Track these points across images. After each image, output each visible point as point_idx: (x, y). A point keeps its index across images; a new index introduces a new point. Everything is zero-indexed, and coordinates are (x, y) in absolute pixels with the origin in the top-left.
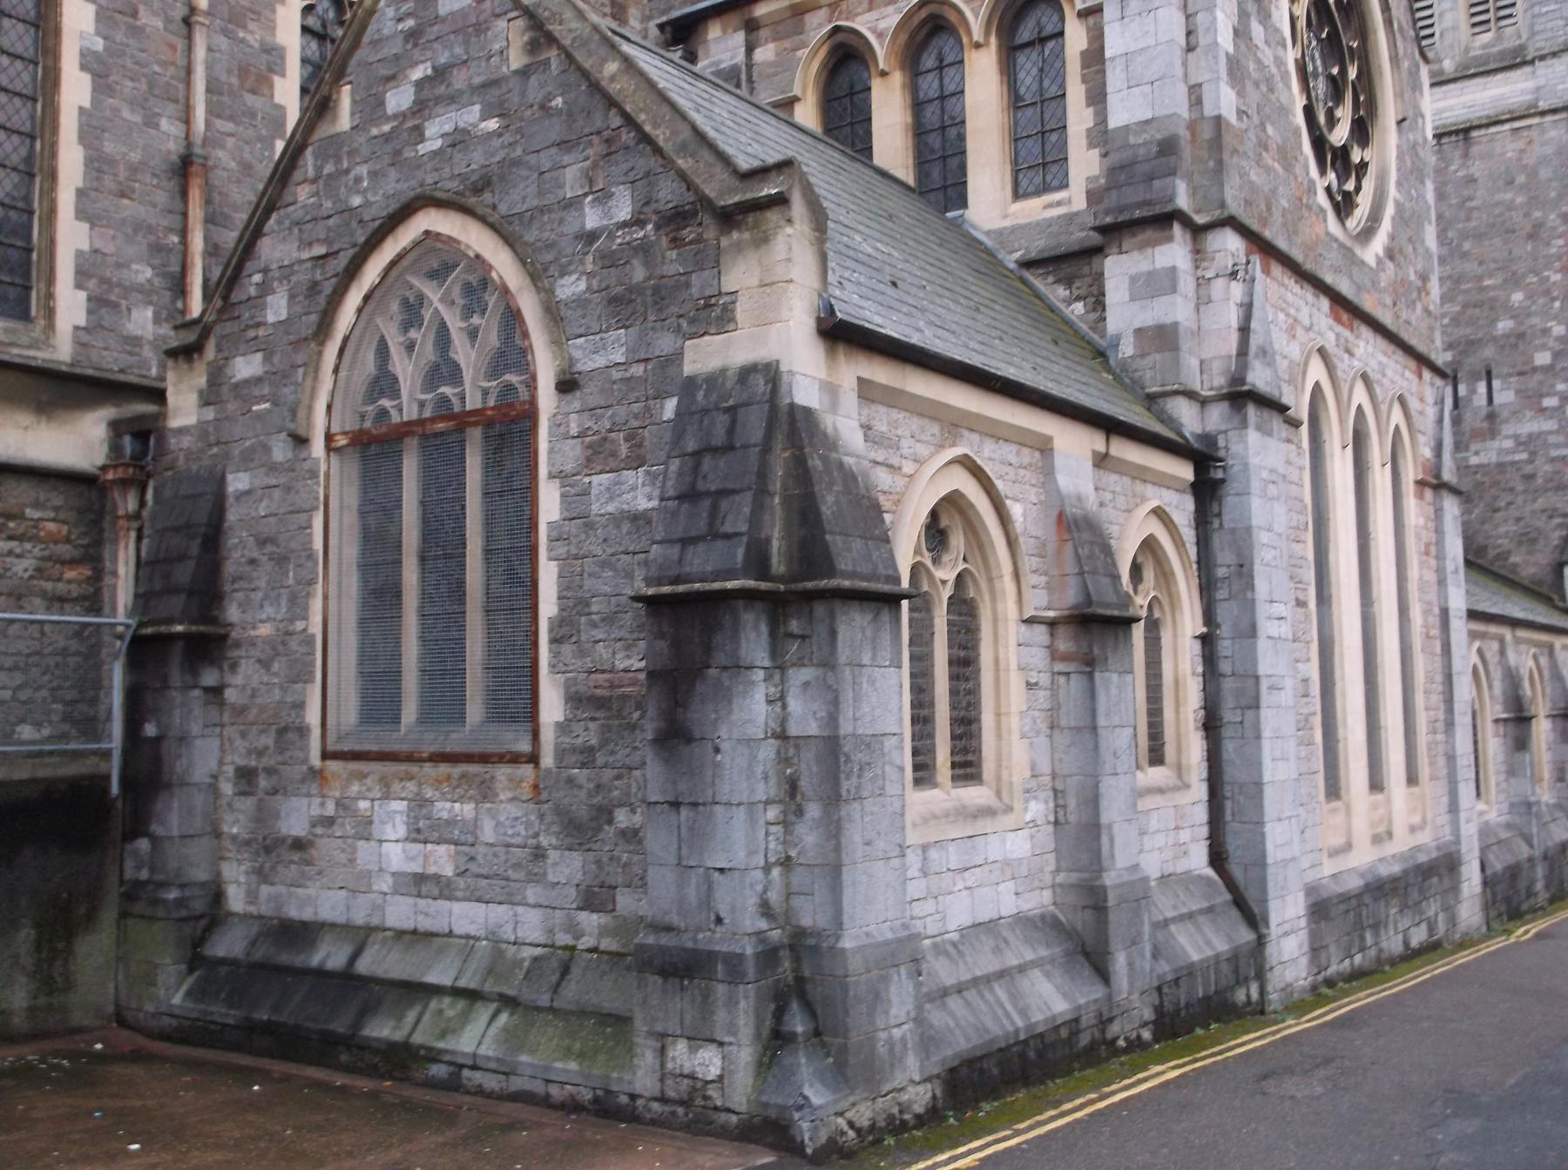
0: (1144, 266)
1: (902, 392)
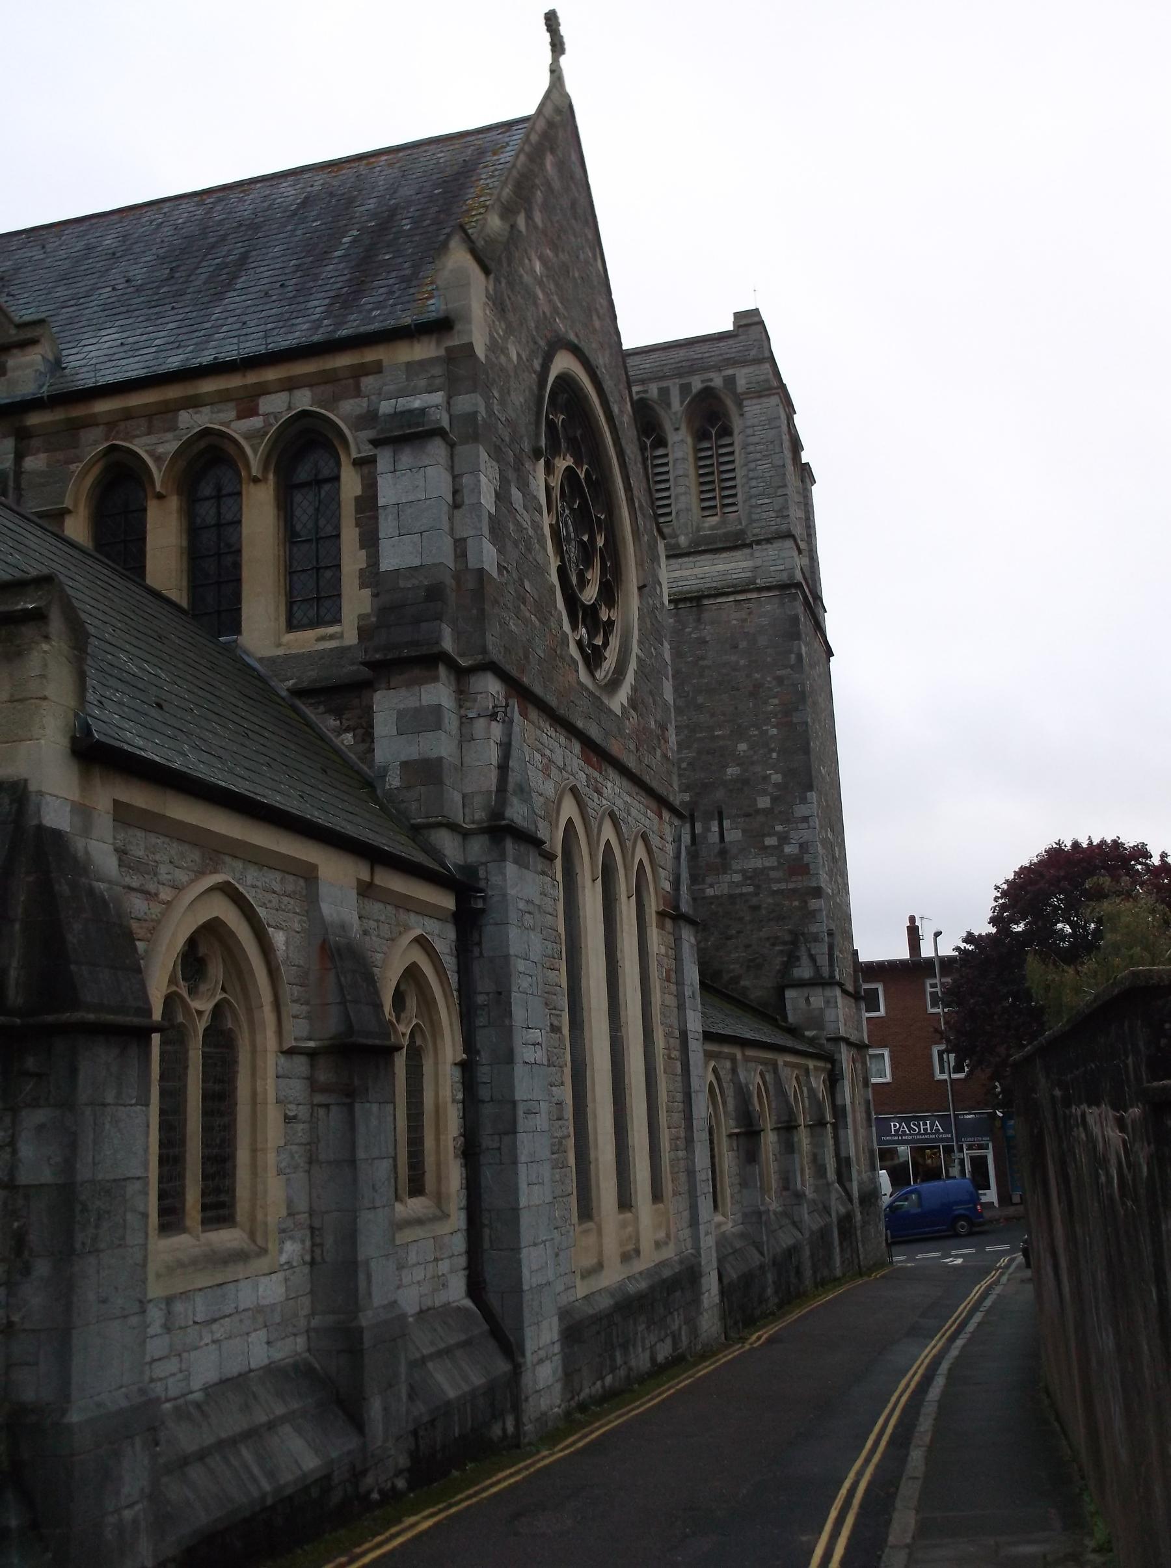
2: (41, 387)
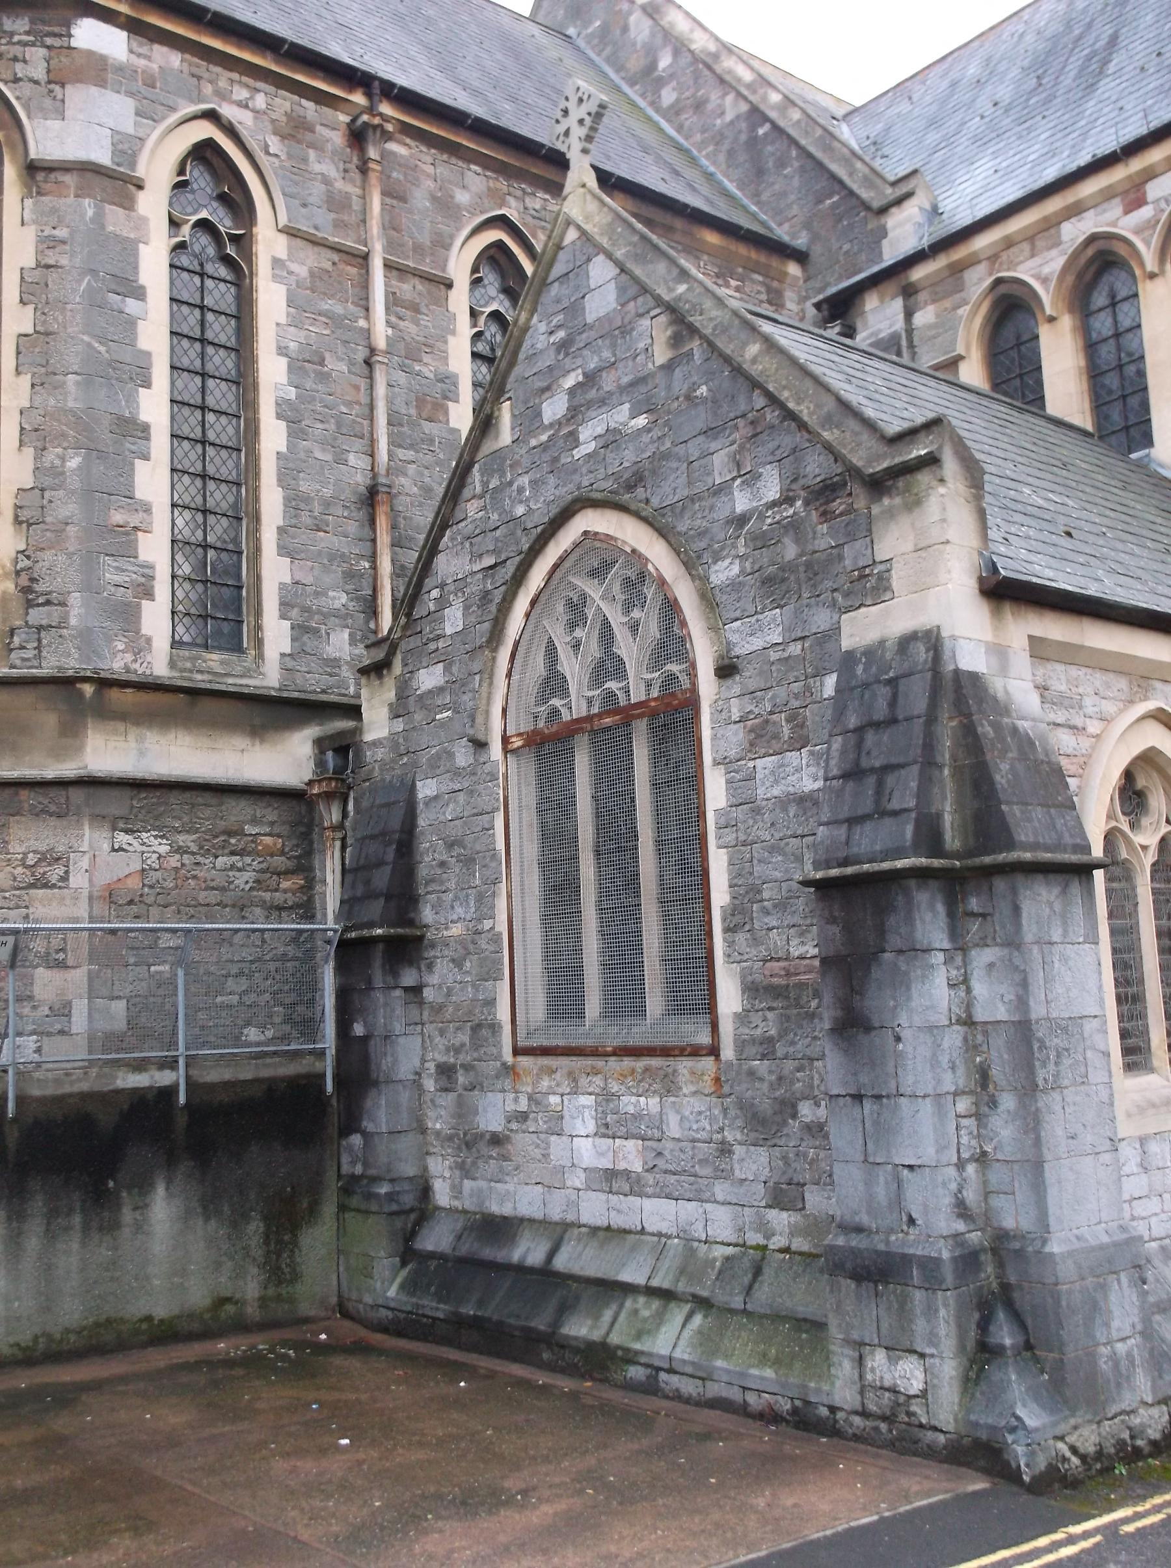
1: (1081, 648)
2: (921, 238)
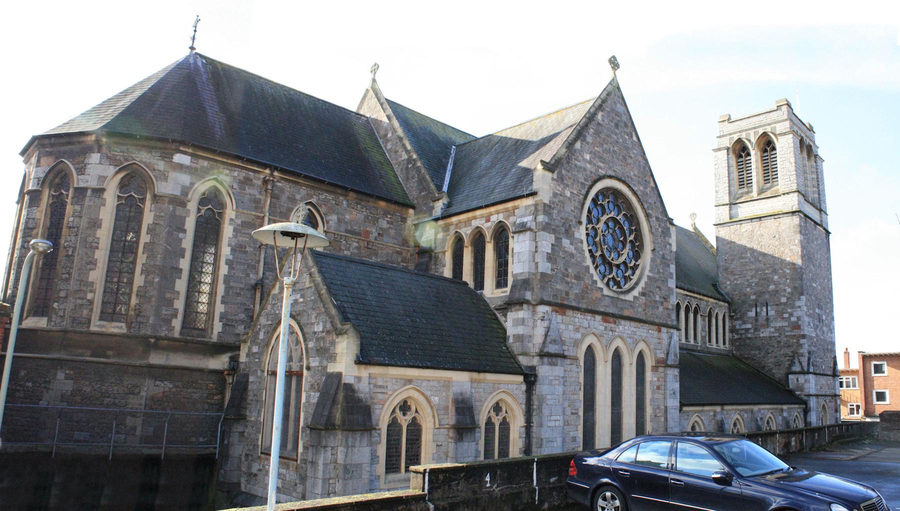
0: (516, 317)
